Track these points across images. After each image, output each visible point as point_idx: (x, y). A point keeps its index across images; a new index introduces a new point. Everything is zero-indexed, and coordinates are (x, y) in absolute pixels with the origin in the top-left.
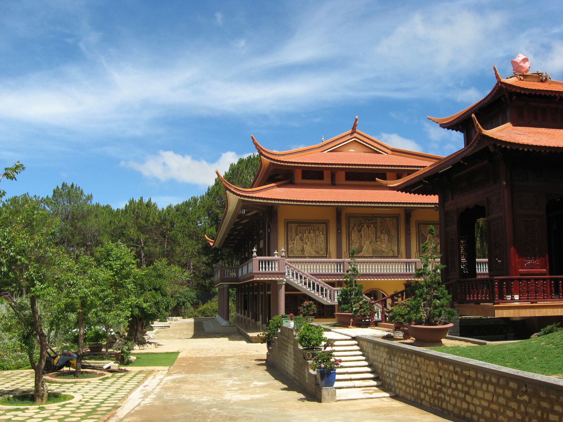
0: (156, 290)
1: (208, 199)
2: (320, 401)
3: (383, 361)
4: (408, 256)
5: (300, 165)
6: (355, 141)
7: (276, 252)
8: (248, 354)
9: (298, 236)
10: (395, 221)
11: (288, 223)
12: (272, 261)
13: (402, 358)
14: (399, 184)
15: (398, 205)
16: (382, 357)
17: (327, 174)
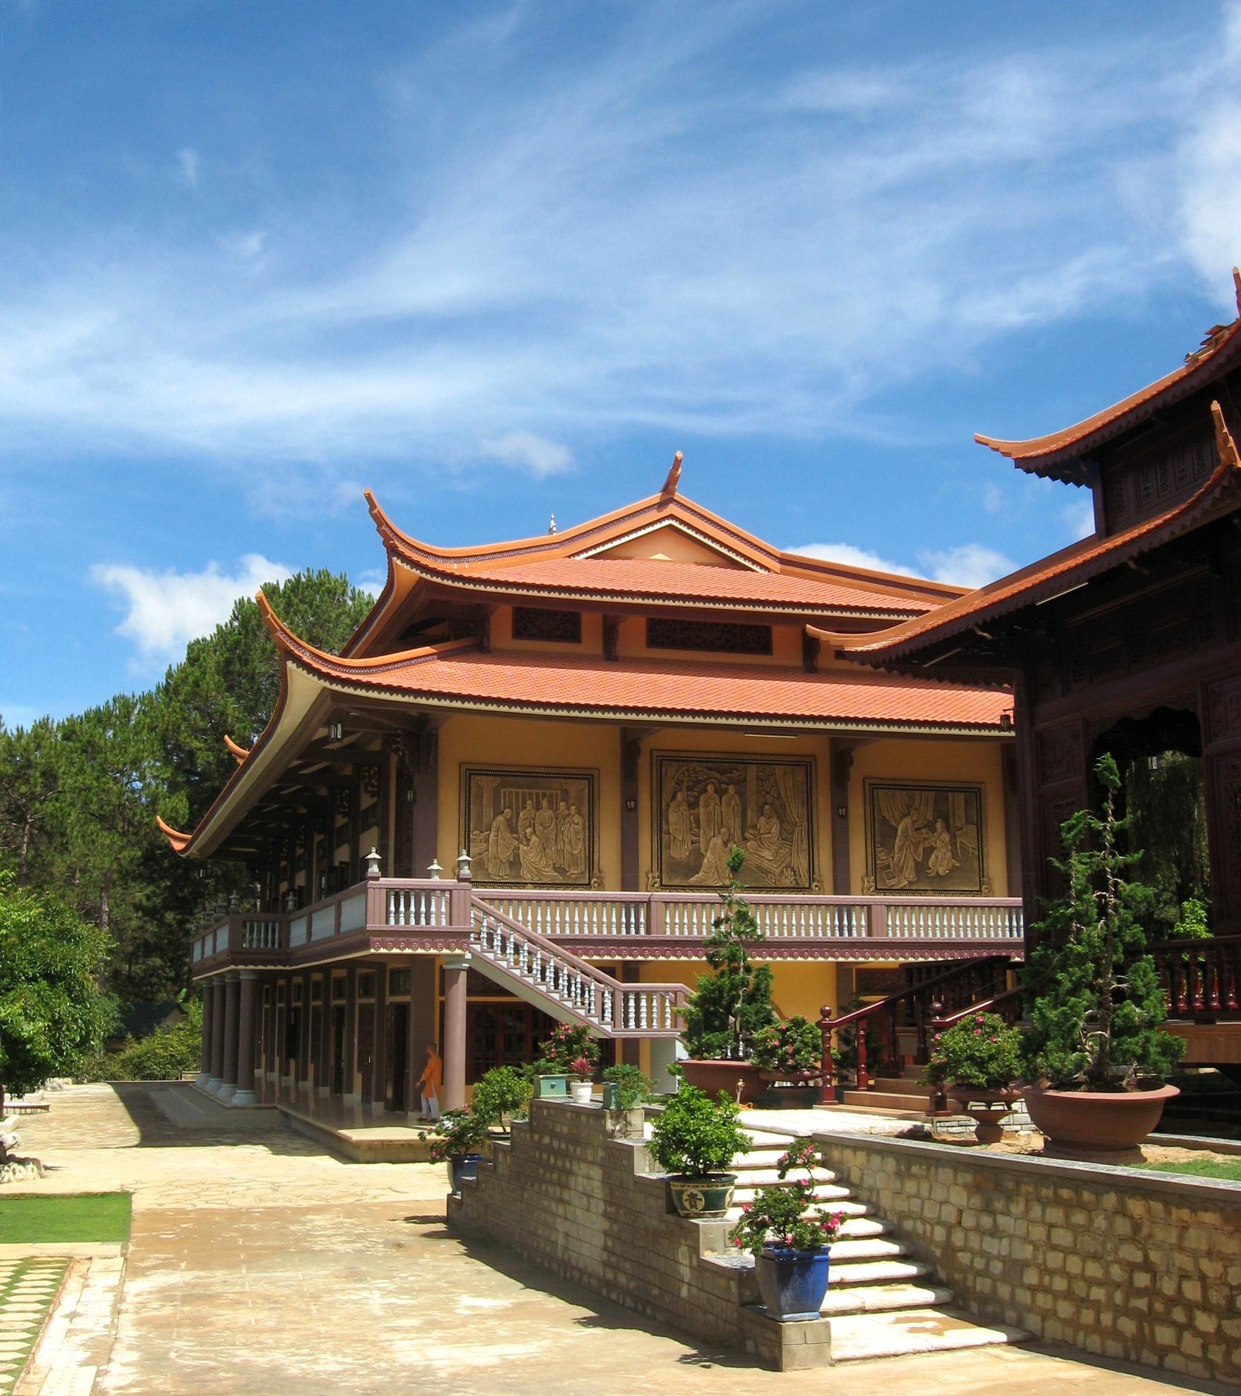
0: (52, 979)
1: (168, 705)
2: (773, 1363)
3: (949, 1214)
4: (841, 886)
5: (514, 591)
6: (670, 526)
7: (435, 867)
8: (367, 1200)
9: (501, 818)
10: (800, 775)
11: (470, 773)
12: (418, 892)
13: (1045, 1204)
14: (884, 643)
15: (821, 726)
16: (946, 1202)
17: (590, 624)
